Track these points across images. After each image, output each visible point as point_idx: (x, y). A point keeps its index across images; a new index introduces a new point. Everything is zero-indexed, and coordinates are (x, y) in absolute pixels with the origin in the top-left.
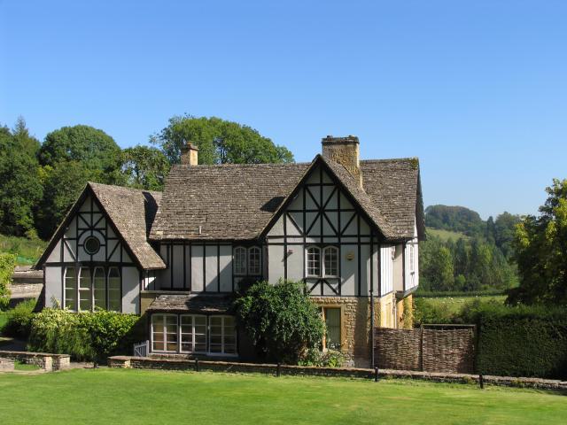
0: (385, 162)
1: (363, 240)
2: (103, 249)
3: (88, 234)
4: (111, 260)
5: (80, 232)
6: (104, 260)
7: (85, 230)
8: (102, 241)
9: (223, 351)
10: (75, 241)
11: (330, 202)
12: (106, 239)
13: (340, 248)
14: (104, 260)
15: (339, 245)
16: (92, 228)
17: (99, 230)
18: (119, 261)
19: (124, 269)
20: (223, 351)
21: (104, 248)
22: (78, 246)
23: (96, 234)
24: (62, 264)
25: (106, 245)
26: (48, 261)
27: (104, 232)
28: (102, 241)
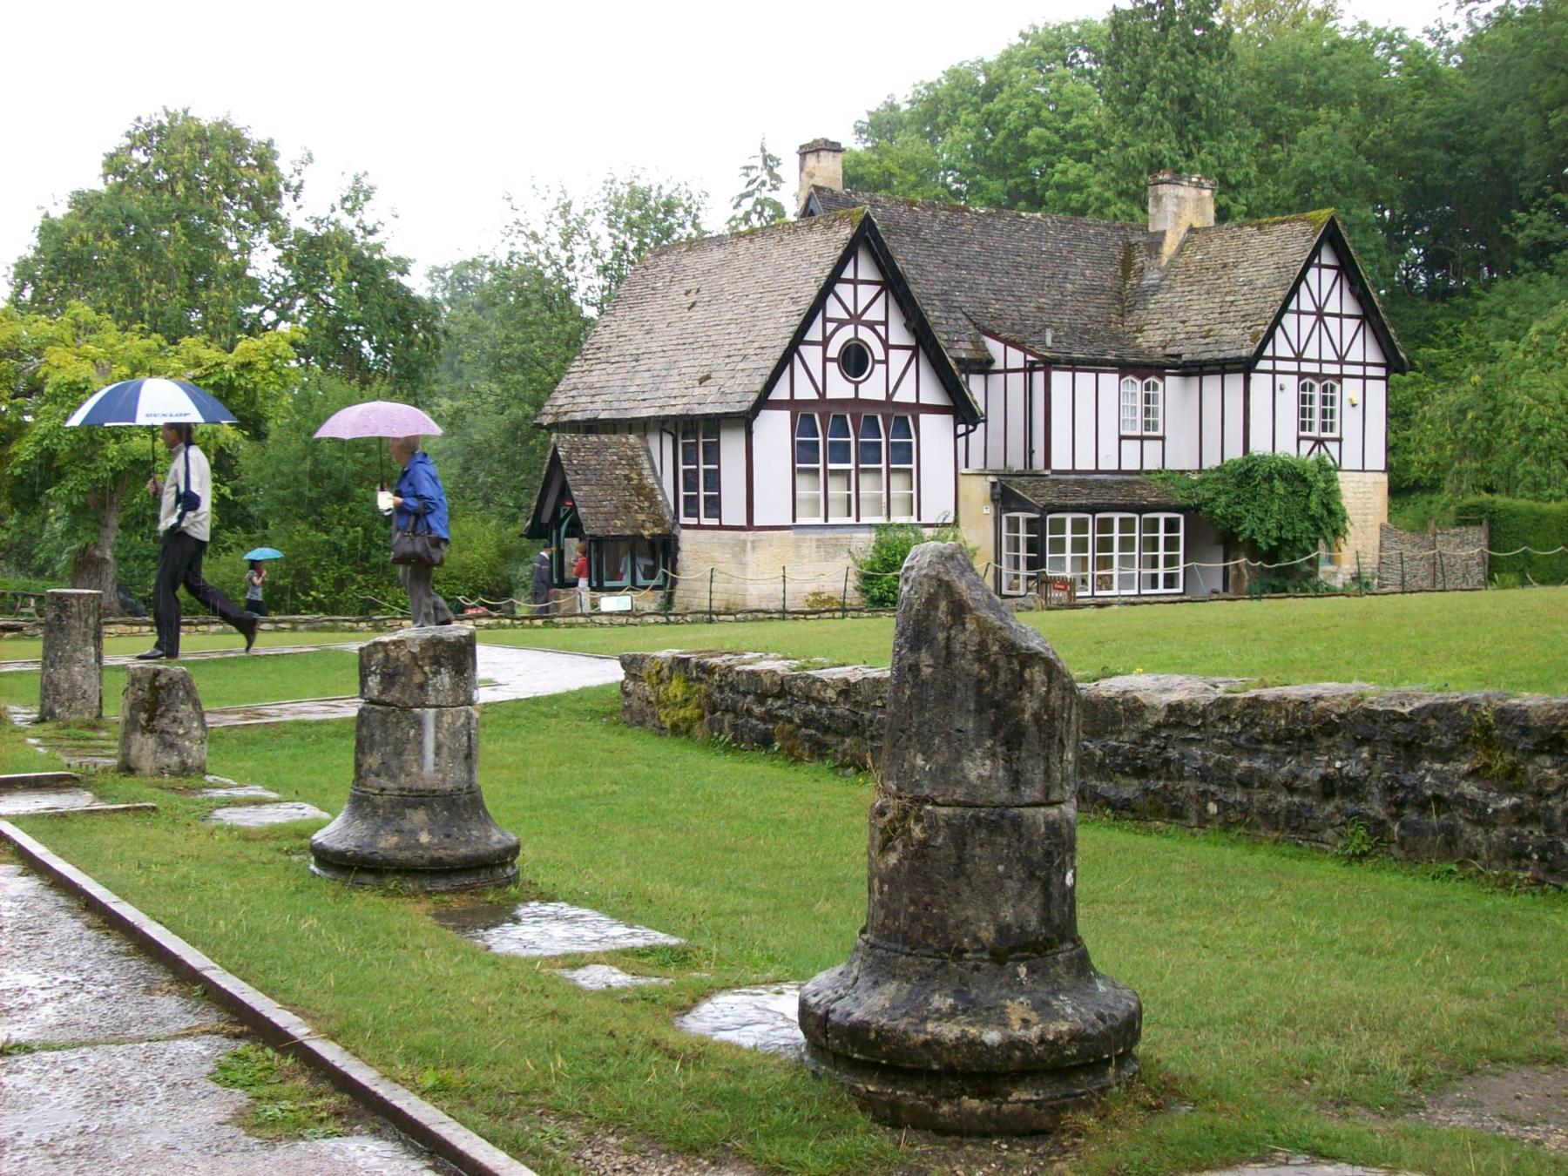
0: (536, 701)
1: (1371, 371)
2: (880, 368)
3: (847, 333)
4: (895, 399)
5: (831, 327)
6: (883, 397)
7: (841, 323)
8: (879, 353)
9: (1154, 571)
10: (820, 348)
11: (27, 886)
12: (887, 347)
13: (1340, 382)
14: (883, 397)
15: (1339, 378)
16: (855, 319)
17: (871, 325)
18: (787, 397)
19: (924, 419)
20: (1154, 571)
21: (829, 355)
22: (825, 360)
23: (865, 334)
24: (792, 404)
25: (886, 362)
26: (773, 397)
27: (881, 329)
28: (879, 353)
